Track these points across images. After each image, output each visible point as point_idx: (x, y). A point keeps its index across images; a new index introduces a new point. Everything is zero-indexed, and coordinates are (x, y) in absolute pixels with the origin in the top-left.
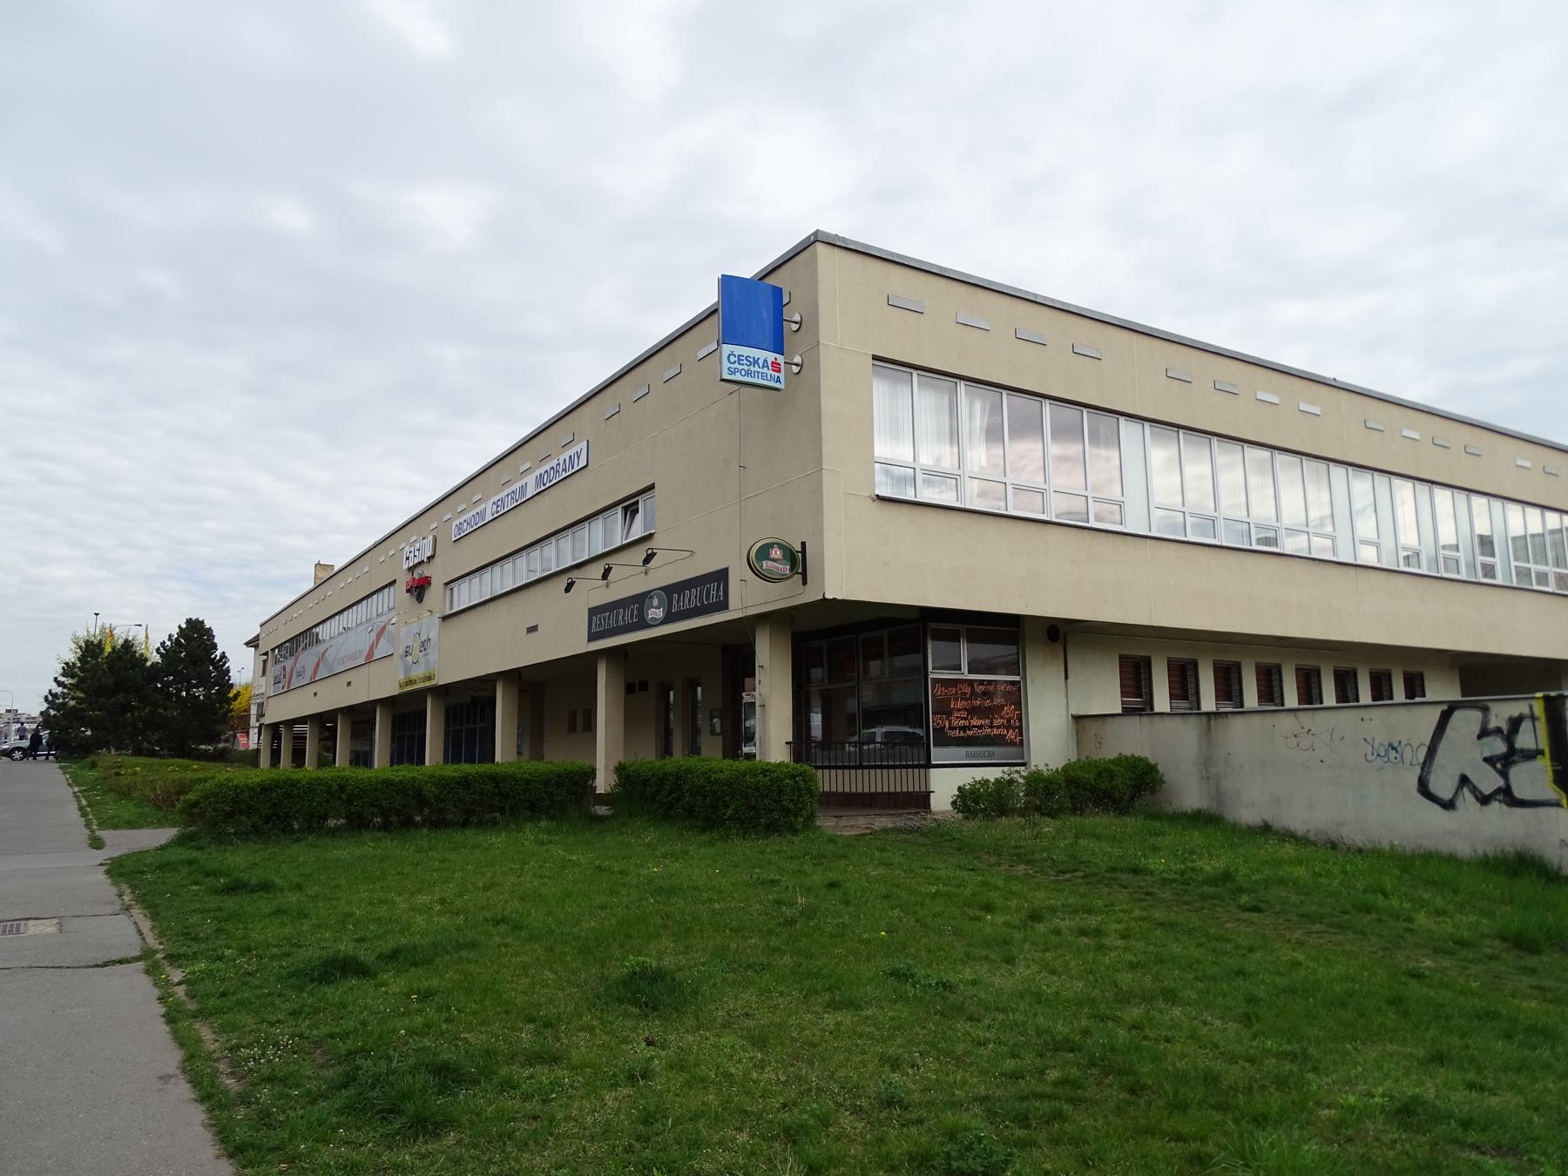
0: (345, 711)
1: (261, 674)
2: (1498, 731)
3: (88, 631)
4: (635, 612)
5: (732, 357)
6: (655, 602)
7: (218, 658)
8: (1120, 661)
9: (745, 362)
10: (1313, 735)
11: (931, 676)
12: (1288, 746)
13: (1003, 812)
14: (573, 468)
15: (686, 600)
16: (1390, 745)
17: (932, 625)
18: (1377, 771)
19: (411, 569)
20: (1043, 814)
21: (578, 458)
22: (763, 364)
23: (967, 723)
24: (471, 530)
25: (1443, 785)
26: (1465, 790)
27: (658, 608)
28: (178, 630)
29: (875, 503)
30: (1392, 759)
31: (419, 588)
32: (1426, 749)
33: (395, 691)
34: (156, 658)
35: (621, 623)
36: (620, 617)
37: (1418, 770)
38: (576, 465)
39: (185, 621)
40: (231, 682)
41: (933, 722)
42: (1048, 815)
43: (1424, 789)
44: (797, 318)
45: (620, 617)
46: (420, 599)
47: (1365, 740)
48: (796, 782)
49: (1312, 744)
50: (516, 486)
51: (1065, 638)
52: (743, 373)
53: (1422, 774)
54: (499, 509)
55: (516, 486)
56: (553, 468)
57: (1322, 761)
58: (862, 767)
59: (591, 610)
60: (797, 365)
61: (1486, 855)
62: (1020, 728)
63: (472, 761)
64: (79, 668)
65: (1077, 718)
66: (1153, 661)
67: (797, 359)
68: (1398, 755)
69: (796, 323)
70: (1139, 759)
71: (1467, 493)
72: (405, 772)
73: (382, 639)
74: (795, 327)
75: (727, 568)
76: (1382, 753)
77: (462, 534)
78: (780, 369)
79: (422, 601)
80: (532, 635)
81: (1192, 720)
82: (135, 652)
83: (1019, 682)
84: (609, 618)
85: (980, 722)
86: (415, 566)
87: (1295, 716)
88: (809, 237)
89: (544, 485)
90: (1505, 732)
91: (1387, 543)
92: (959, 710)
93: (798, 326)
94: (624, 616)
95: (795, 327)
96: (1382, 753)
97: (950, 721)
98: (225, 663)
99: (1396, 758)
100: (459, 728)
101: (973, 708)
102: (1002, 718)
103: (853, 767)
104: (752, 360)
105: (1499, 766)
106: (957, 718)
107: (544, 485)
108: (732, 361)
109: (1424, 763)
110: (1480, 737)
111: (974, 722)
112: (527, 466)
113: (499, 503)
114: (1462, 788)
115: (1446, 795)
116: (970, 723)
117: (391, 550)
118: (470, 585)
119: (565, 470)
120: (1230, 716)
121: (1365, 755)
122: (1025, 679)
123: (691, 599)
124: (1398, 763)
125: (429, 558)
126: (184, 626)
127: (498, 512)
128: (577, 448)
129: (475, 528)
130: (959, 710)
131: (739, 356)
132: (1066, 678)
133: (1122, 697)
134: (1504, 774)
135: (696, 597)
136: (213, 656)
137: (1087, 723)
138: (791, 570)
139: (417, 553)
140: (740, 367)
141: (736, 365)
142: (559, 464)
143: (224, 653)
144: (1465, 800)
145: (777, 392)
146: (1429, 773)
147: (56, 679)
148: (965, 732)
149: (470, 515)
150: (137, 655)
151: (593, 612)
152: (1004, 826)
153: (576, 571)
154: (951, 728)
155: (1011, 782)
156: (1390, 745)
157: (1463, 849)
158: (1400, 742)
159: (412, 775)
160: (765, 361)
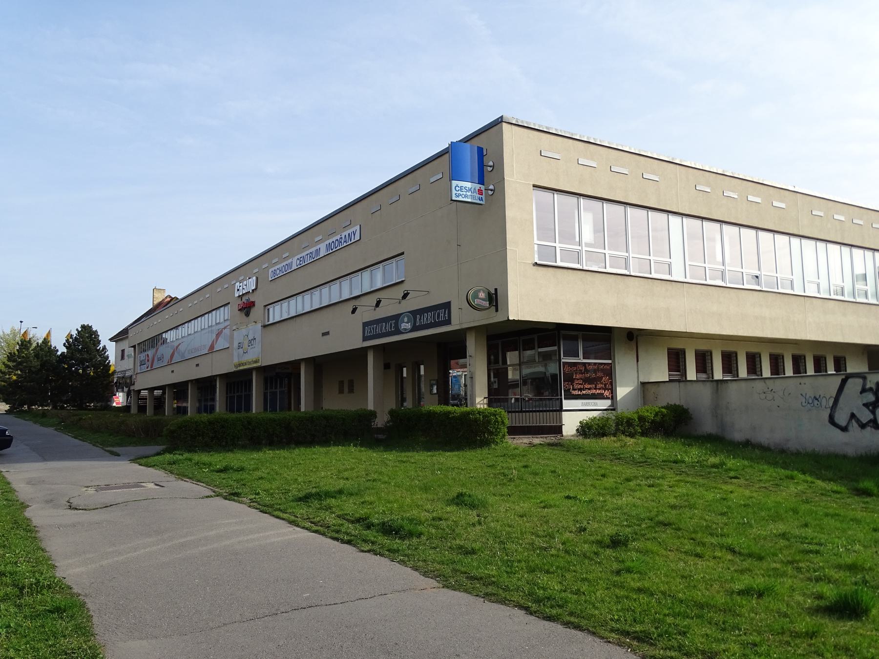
0: (194, 382)
1: (120, 359)
2: (871, 389)
3: (3, 332)
4: (393, 325)
5: (457, 187)
6: (406, 320)
7: (101, 349)
8: (668, 352)
9: (464, 190)
10: (774, 392)
11: (563, 361)
12: (760, 398)
13: (604, 435)
14: (351, 241)
15: (425, 319)
16: (815, 397)
17: (563, 332)
18: (808, 411)
19: (240, 297)
20: (626, 435)
21: (354, 235)
22: (474, 192)
23: (582, 387)
24: (282, 274)
25: (842, 418)
26: (853, 421)
27: (407, 323)
28: (76, 332)
29: (535, 267)
30: (816, 405)
31: (247, 308)
32: (833, 400)
33: (233, 369)
34: (62, 350)
35: (384, 331)
36: (383, 328)
37: (829, 411)
38: (353, 239)
39: (80, 326)
40: (110, 364)
41: (564, 387)
42: (629, 436)
43: (832, 421)
44: (491, 163)
45: (383, 328)
46: (247, 314)
47: (801, 394)
48: (497, 418)
49: (773, 397)
50: (313, 249)
51: (637, 339)
52: (463, 196)
53: (831, 413)
54: (301, 263)
55: (313, 249)
56: (337, 240)
57: (778, 406)
58: (521, 412)
59: (364, 324)
60: (491, 190)
61: (862, 455)
62: (612, 390)
63: (239, 411)
64: (18, 356)
65: (643, 384)
66: (686, 351)
67: (491, 187)
68: (818, 403)
69: (491, 167)
70: (679, 406)
71: (873, 251)
72: (205, 417)
73: (220, 338)
74: (490, 169)
75: (450, 302)
76: (811, 402)
77: (276, 277)
78: (482, 193)
79: (248, 316)
80: (325, 337)
81: (708, 384)
82: (51, 346)
83: (611, 364)
84: (376, 328)
85: (589, 386)
86: (243, 295)
87: (765, 382)
88: (498, 119)
89: (332, 250)
90: (874, 390)
91: (824, 285)
92: (578, 379)
93: (492, 168)
94: (386, 327)
95: (490, 169)
96: (811, 402)
97: (573, 386)
98: (106, 352)
99: (817, 404)
100: (275, 390)
101: (586, 378)
102: (602, 383)
103: (517, 412)
104: (467, 189)
105: (871, 408)
106: (577, 384)
107: (332, 250)
108: (457, 190)
109: (832, 406)
110: (861, 393)
111: (586, 386)
112: (320, 238)
113: (301, 259)
114: (852, 420)
115: (843, 423)
116: (584, 387)
117: (226, 284)
118: (281, 306)
119: (345, 242)
120: (729, 382)
121: (802, 403)
122: (614, 361)
123: (428, 318)
124: (818, 407)
125: (253, 290)
126: (80, 329)
127: (300, 264)
128: (354, 229)
129: (285, 273)
130: (578, 379)
131: (461, 187)
132: (638, 361)
133: (669, 371)
134: (873, 412)
135: (431, 317)
136: (98, 348)
137: (649, 386)
138: (489, 304)
139: (245, 287)
140: (461, 193)
141: (459, 192)
142: (341, 238)
143: (105, 346)
144: (853, 426)
145: (480, 206)
146: (835, 412)
147: (4, 363)
148: (581, 391)
149: (282, 265)
150: (52, 348)
151: (365, 325)
152: (607, 442)
153: (354, 300)
154: (574, 389)
155: (608, 419)
156: (815, 397)
157: (850, 451)
158: (820, 396)
159: (284, 416)
160: (475, 189)
